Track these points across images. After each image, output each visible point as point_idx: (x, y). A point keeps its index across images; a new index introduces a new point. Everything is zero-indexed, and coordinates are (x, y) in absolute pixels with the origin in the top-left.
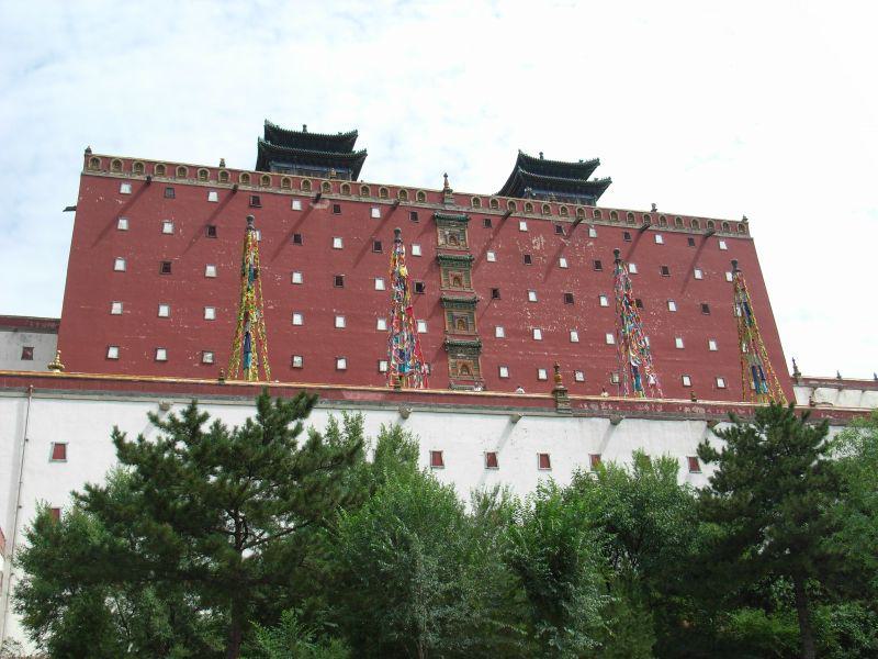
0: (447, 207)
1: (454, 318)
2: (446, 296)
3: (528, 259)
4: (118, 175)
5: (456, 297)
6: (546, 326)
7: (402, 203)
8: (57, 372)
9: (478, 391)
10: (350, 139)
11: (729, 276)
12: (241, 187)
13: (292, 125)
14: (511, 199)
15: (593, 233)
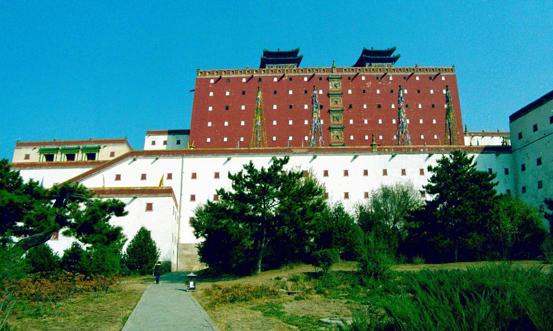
0: (334, 74)
1: (334, 117)
2: (331, 109)
3: (364, 92)
4: (209, 77)
5: (335, 109)
6: (369, 118)
7: (316, 74)
8: (192, 148)
9: (278, 148)
10: (297, 51)
11: (444, 92)
12: (223, 76)
13: (369, 49)
14: (359, 68)
15: (391, 78)
